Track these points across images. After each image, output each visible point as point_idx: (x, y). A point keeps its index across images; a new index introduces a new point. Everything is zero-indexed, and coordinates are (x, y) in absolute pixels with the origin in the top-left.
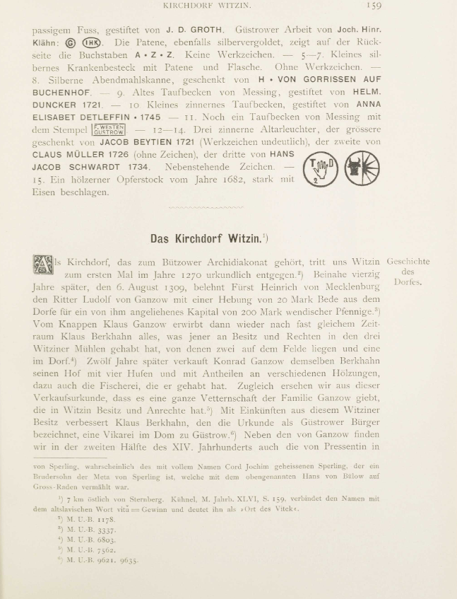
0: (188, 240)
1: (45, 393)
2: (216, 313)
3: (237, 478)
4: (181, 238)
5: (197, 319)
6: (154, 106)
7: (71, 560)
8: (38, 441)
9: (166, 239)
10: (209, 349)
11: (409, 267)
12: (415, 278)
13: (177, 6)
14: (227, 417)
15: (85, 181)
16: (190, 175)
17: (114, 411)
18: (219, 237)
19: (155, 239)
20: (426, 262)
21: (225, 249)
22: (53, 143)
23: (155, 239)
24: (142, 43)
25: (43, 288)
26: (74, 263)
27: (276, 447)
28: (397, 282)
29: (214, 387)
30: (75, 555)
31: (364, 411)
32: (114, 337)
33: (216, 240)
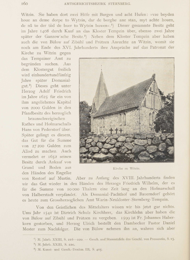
2: (107, 195)
3: (102, 229)
5: (38, 62)
6: (120, 37)
13: (127, 4)
14: (34, 187)
15: (89, 213)
22: (71, 208)
24: (153, 48)
25: (147, 229)
26: (96, 213)
27: (163, 229)
29: (163, 20)
31: (53, 53)
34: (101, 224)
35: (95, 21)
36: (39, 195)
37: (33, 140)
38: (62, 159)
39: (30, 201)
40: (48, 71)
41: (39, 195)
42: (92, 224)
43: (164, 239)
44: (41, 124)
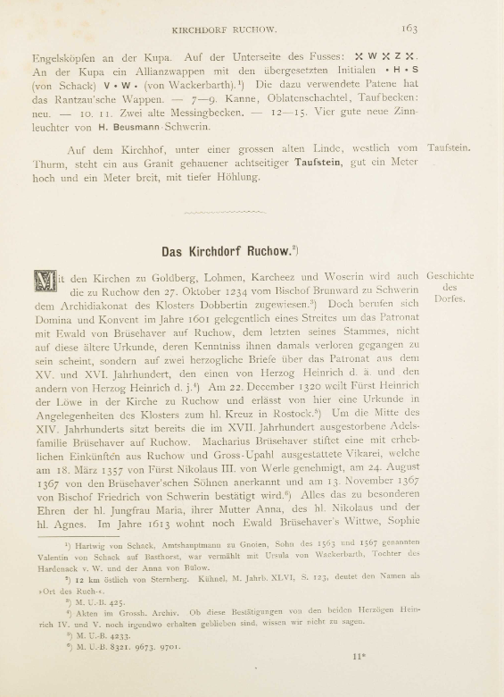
0: (204, 253)
1: (46, 314)
4: (195, 251)
7: (80, 647)
8: (42, 328)
9: (179, 253)
10: (185, 347)
11: (452, 282)
12: (457, 294)
16: (391, 106)
17: (85, 362)
18: (238, 249)
19: (167, 252)
20: (468, 277)
21: (241, 264)
23: (167, 252)
28: (438, 299)
30: (86, 642)
32: (81, 307)
33: (235, 253)
34: (221, 497)
35: (305, 360)
36: (161, 557)
37: (155, 277)
38: (161, 329)
39: (139, 178)
40: (106, 455)
41: (161, 557)
42: (228, 524)
43: (263, 578)
44: (91, 321)
